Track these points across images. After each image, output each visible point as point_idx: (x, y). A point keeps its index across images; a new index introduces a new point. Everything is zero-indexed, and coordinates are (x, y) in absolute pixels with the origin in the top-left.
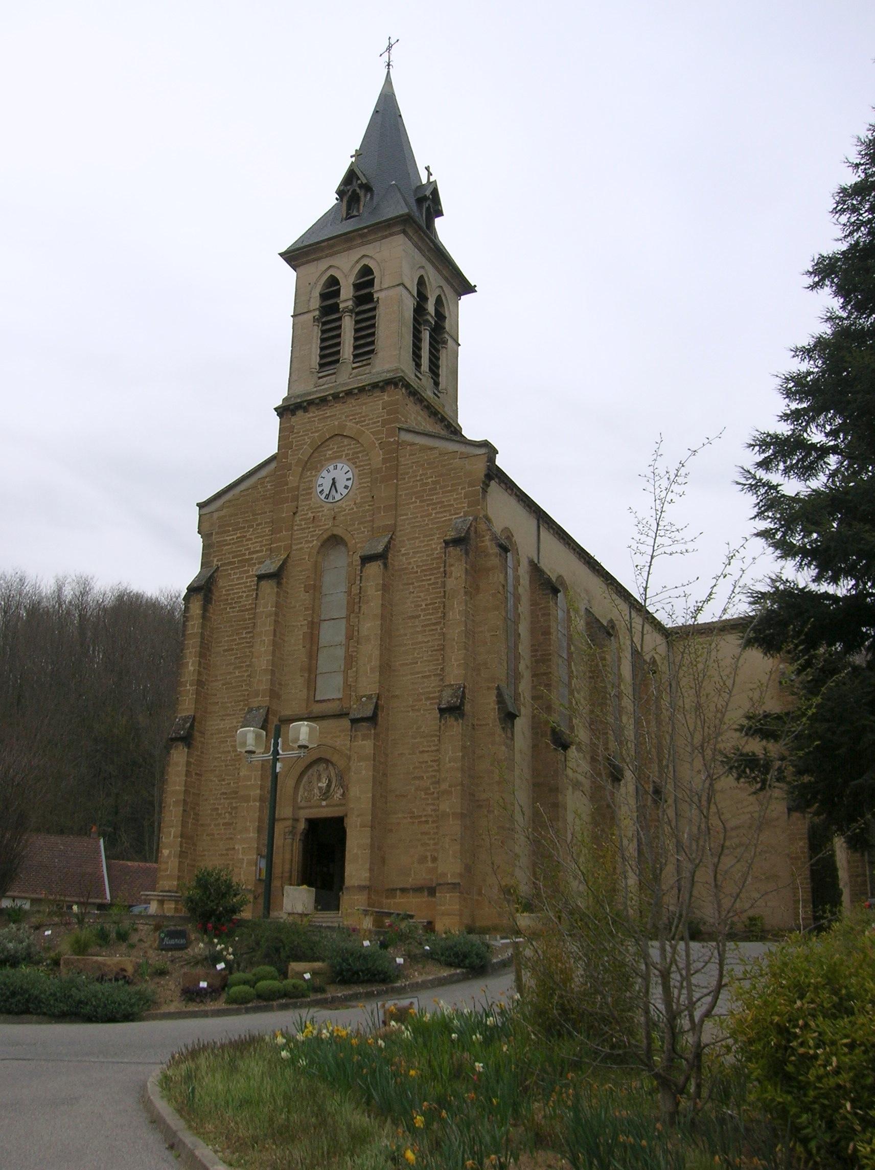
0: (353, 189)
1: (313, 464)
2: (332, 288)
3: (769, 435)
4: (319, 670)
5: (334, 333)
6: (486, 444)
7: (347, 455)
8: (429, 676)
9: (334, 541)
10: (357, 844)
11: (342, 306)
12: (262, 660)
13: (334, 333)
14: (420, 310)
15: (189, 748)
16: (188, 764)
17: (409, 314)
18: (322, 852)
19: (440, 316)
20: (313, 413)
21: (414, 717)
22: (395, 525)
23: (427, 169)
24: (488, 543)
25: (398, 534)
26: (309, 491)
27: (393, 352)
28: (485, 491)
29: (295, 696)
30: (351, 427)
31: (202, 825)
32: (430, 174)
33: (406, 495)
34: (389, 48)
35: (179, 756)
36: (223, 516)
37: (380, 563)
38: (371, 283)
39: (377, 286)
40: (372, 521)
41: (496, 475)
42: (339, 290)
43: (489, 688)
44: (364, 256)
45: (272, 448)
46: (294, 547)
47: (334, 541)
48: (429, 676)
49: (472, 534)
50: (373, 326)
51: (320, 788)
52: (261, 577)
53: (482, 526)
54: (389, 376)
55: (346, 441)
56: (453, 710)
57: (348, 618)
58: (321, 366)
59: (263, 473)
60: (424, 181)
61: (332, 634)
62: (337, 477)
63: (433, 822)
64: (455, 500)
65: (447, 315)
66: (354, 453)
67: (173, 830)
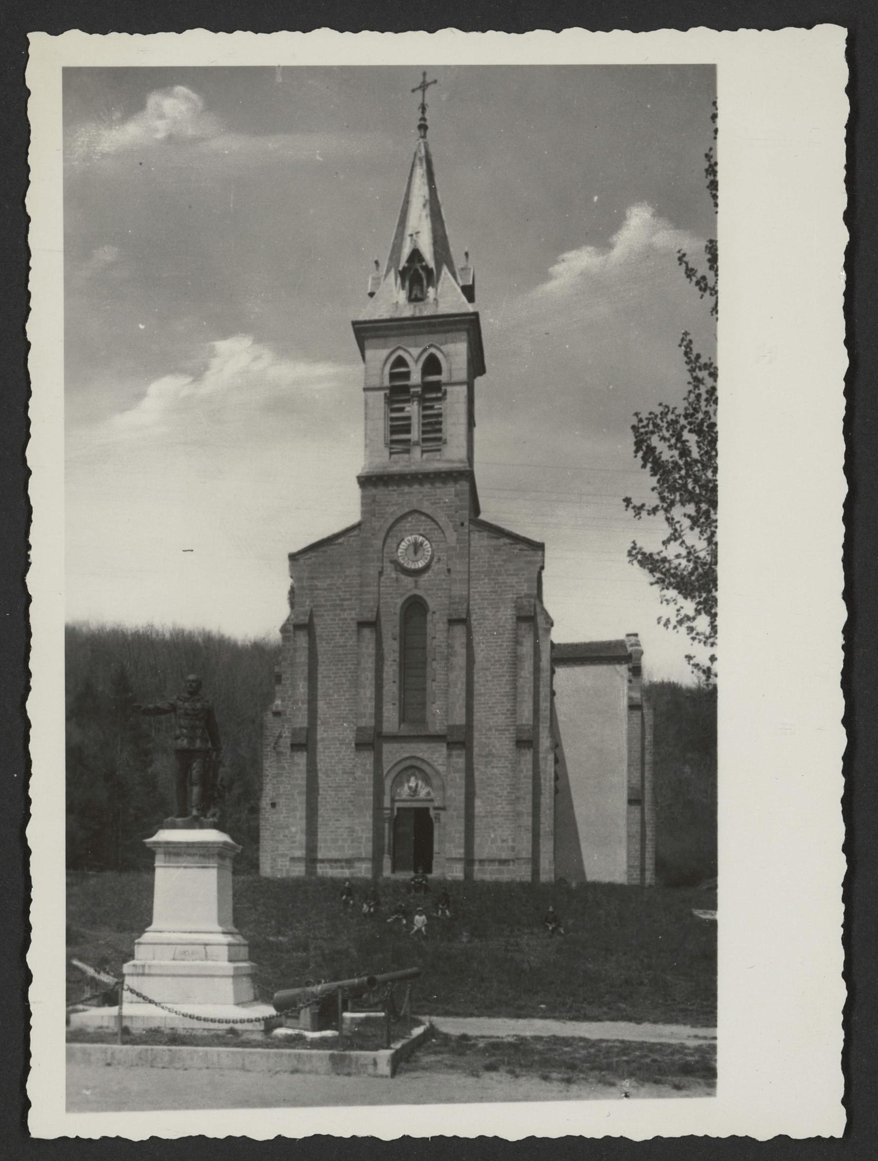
11: (412, 390)
33: (476, 572)
38: (438, 370)
51: (410, 788)
55: (423, 518)
63: (502, 816)
64: (517, 583)
66: (430, 529)
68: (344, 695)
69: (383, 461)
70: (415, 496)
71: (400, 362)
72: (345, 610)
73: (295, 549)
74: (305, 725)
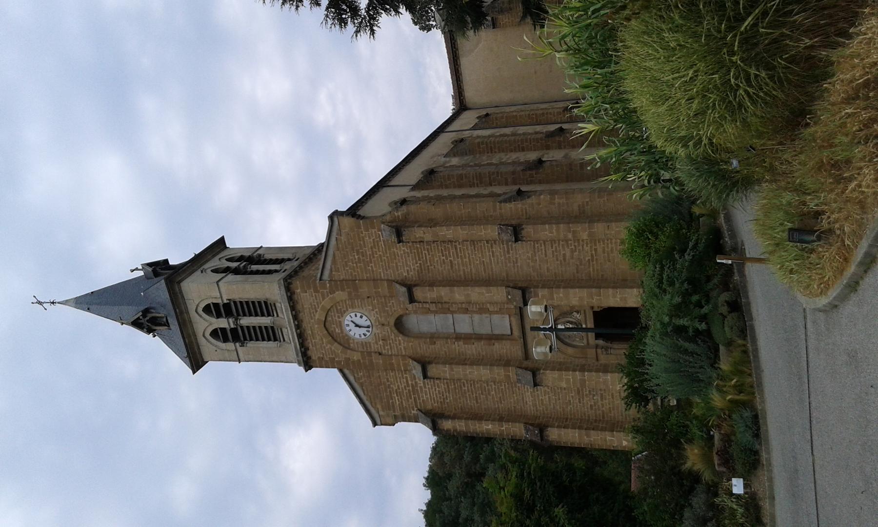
0: (147, 322)
1: (345, 342)
2: (219, 334)
3: (327, 16)
4: (490, 332)
5: (252, 331)
6: (331, 217)
7: (339, 317)
8: (493, 252)
9: (399, 325)
10: (614, 299)
11: (232, 326)
12: (482, 373)
13: (252, 331)
14: (236, 271)
15: (548, 427)
16: (559, 427)
17: (239, 277)
18: (614, 324)
19: (241, 259)
20: (310, 344)
21: (523, 259)
22: (388, 280)
23: (132, 271)
24: (400, 213)
25: (393, 278)
26: (365, 344)
27: (268, 289)
28: (363, 218)
29: (514, 350)
30: (319, 315)
31: (603, 417)
32: (137, 269)
34: (40, 303)
35: (555, 435)
36: (382, 409)
37: (414, 289)
38: (216, 305)
39: (219, 301)
40: (385, 297)
41: (354, 211)
42: (221, 329)
43: (501, 209)
44: (196, 311)
45: (334, 373)
46: (404, 353)
47: (399, 325)
48: (493, 252)
49: (394, 224)
50: (247, 303)
52: (425, 376)
53: (388, 218)
54: (283, 289)
55: (329, 319)
56: (517, 234)
57: (452, 313)
58: (275, 340)
59: (352, 378)
60: (141, 273)
61: (464, 324)
62: (357, 325)
63: (595, 245)
64: (370, 238)
65: (239, 255)
67: (608, 438)
69: (291, 346)
71: (215, 334)
72: (416, 383)
74: (522, 426)
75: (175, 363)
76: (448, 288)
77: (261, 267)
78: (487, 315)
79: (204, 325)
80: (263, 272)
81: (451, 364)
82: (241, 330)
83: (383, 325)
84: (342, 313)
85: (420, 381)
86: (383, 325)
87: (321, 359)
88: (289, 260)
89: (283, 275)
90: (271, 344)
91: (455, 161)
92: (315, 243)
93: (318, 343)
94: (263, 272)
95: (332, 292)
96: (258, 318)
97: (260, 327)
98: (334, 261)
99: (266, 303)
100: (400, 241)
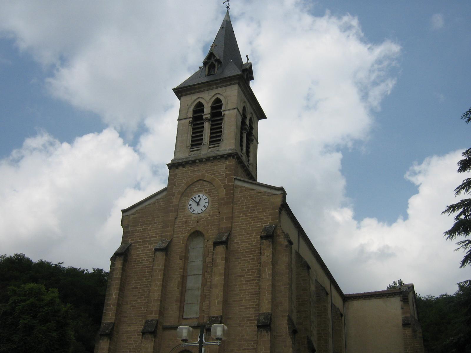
0: (211, 62)
1: (187, 193)
2: (199, 108)
6: (281, 189)
8: (249, 308)
9: (196, 234)
11: (204, 117)
12: (156, 294)
14: (243, 122)
15: (110, 340)
17: (239, 123)
22: (231, 227)
23: (247, 56)
27: (229, 143)
32: (248, 60)
38: (221, 107)
39: (223, 108)
41: (285, 207)
44: (217, 93)
46: (175, 236)
47: (196, 234)
48: (249, 308)
50: (221, 128)
52: (156, 250)
55: (205, 183)
57: (203, 275)
58: (192, 145)
59: (159, 197)
61: (194, 283)
62: (199, 205)
65: (254, 127)
68: (144, 300)
70: (202, 170)
72: (152, 244)
73: (125, 208)
74: (113, 321)
75: (182, 77)
76: (223, 271)
77: (245, 140)
78: (199, 301)
79: (207, 99)
80: (241, 141)
81: (164, 270)
82: (201, 123)
83: (197, 222)
84: (209, 193)
85: (153, 247)
86: (197, 222)
87: (175, 176)
88: (249, 160)
89: (240, 154)
90: (189, 142)
91: (313, 288)
92: (257, 180)
93: (187, 174)
94: (241, 141)
95: (225, 186)
96: (209, 135)
97: (202, 135)
98: (248, 189)
99: (220, 140)
100: (262, 238)
